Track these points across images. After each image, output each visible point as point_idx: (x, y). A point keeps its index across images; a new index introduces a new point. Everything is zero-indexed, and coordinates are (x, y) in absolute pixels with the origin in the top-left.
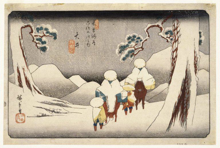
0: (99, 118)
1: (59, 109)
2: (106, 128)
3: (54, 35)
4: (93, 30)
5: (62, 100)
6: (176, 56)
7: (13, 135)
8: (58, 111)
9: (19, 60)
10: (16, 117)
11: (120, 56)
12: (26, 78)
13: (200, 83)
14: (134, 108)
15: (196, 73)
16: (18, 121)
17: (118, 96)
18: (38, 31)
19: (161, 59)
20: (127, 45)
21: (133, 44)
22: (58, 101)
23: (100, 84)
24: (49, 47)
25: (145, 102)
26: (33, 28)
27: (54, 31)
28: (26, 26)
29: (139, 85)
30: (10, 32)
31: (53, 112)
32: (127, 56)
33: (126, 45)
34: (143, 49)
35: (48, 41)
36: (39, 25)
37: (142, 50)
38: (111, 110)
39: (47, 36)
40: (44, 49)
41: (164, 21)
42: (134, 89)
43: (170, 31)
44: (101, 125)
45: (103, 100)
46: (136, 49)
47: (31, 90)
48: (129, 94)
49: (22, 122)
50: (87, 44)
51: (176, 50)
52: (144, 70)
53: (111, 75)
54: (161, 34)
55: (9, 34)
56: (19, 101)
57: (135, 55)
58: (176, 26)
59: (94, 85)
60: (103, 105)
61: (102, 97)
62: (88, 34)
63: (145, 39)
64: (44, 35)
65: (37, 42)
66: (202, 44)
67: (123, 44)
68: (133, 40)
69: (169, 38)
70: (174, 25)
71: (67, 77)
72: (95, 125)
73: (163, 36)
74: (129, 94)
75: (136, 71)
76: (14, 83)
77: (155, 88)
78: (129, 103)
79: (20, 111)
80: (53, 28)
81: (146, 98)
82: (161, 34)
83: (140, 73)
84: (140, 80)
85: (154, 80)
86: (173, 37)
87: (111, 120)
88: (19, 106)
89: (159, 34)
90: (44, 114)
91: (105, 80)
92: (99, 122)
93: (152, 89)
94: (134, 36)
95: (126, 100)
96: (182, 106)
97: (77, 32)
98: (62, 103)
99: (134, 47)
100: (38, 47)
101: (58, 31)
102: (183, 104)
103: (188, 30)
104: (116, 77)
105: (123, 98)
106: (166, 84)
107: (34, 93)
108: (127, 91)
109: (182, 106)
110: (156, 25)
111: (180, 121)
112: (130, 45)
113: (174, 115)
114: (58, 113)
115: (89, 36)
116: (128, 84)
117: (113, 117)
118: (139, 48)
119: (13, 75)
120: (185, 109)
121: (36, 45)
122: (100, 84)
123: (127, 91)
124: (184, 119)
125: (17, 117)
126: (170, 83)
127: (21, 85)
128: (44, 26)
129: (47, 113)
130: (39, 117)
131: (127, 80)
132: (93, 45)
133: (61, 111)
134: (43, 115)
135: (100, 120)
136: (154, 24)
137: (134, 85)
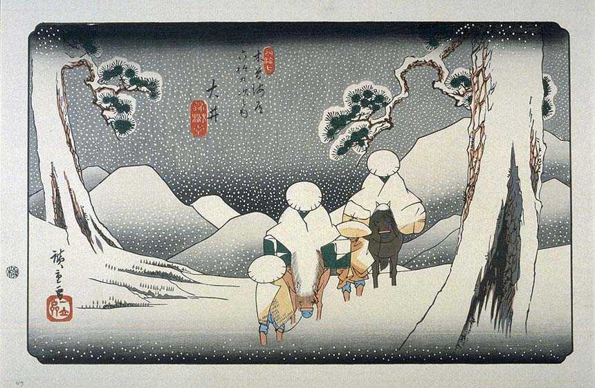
9: (56, 152)
16: (54, 316)
19: (437, 157)
25: (399, 268)
29: (382, 220)
49: (65, 317)
59: (257, 222)
67: (336, 110)
75: (371, 183)
84: (384, 208)
91: (289, 208)
96: (500, 275)
103: (514, 74)
109: (500, 275)
113: (478, 299)
116: (353, 218)
127: (60, 222)
131: (350, 208)
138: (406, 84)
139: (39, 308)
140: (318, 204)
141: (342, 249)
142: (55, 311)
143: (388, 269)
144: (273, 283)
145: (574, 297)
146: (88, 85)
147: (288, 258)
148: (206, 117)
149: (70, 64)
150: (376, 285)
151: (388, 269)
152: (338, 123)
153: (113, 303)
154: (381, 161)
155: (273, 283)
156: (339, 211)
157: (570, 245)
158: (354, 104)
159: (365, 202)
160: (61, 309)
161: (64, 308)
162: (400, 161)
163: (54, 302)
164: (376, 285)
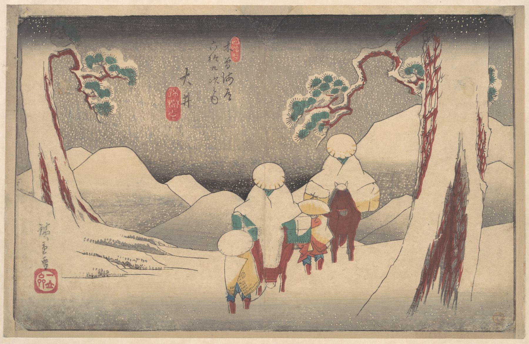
0: (241, 281)
1: (141, 258)
2: (255, 312)
3: (130, 73)
4: (227, 62)
5: (148, 238)
6: (434, 130)
7: (29, 320)
8: (139, 263)
9: (43, 137)
10: (35, 277)
11: (293, 128)
12: (62, 183)
13: (490, 196)
14: (327, 257)
15: (482, 171)
16: (41, 288)
17: (289, 228)
18: (90, 66)
19: (394, 139)
20: (311, 101)
21: (325, 98)
22: (139, 239)
23: (244, 196)
24: (118, 105)
25: (356, 243)
26: (79, 57)
27: (131, 64)
28: (61, 54)
29: (341, 199)
30: (20, 82)
31: (126, 267)
32: (309, 126)
33: (307, 100)
34: (351, 110)
35: (115, 89)
36: (94, 50)
37: (350, 114)
38: (271, 261)
39: (113, 78)
40: (106, 109)
41: (403, 43)
42: (327, 210)
43: (418, 67)
44: (247, 300)
45: (250, 238)
46: (333, 111)
47: (73, 209)
48: (316, 222)
49: (51, 289)
50: (212, 98)
51: (434, 113)
52: (352, 163)
53: (269, 175)
54: (394, 73)
55: (19, 74)
56: (42, 239)
57: (332, 125)
58: (432, 53)
59: (226, 201)
60: (253, 250)
61: (246, 229)
62: (213, 72)
63: (353, 87)
64: (108, 75)
65: (88, 91)
66: (496, 99)
67: (299, 97)
68: (325, 87)
69: (416, 83)
70: (429, 53)
71: (163, 178)
72: (231, 299)
73: (400, 79)
74: (316, 222)
75: (331, 163)
76: (32, 194)
77: (379, 208)
78: (315, 244)
79: (45, 261)
80: (125, 59)
81: (358, 235)
82: (394, 73)
83: (347, 166)
84: (341, 188)
85: (377, 189)
86: (429, 70)
87: (271, 289)
88: (41, 251)
89: (391, 73)
90: (105, 269)
91: (255, 186)
92: (241, 293)
93: (371, 210)
94: (328, 79)
95: (308, 237)
96: (446, 255)
97: (187, 69)
98: (149, 243)
99: (328, 106)
100: (89, 105)
101: (139, 66)
102: (450, 249)
103: (463, 66)
104: (283, 179)
105: (301, 233)
106: (407, 199)
107: (80, 221)
108: (311, 216)
109: (446, 255)
110: (383, 51)
111: (440, 292)
112: (318, 99)
113: (427, 277)
114: (137, 268)
115: (216, 78)
116: (313, 197)
117: (274, 280)
118: (342, 108)
119: (26, 176)
120: (456, 260)
121: (86, 100)
122: (244, 196)
123: (311, 216)
124: (449, 289)
125: (38, 278)
126: (416, 195)
127: (48, 200)
128: (106, 53)
129: (112, 268)
130: (92, 277)
131: (310, 187)
132: (226, 100)
133: (146, 265)
134: (103, 274)
135: (241, 286)
136: (376, 50)
137: (327, 201)
138: (363, 73)
139: (27, 283)
140: (281, 184)
141: (303, 225)
142: (42, 283)
143: (345, 245)
144: (239, 256)
145: (517, 269)
146: (73, 73)
147: (254, 232)
148: (180, 103)
149: (56, 53)
150: (334, 260)
151: (345, 245)
152: (298, 109)
153: (95, 273)
154: (339, 143)
155: (239, 256)
156: (301, 190)
157: (513, 223)
158: (315, 98)
159: (324, 184)
160: (47, 282)
161: (50, 281)
162: (356, 144)
163: (42, 275)
164: (334, 260)
